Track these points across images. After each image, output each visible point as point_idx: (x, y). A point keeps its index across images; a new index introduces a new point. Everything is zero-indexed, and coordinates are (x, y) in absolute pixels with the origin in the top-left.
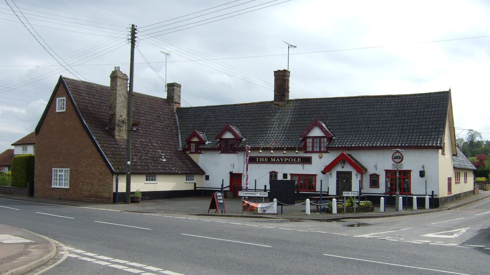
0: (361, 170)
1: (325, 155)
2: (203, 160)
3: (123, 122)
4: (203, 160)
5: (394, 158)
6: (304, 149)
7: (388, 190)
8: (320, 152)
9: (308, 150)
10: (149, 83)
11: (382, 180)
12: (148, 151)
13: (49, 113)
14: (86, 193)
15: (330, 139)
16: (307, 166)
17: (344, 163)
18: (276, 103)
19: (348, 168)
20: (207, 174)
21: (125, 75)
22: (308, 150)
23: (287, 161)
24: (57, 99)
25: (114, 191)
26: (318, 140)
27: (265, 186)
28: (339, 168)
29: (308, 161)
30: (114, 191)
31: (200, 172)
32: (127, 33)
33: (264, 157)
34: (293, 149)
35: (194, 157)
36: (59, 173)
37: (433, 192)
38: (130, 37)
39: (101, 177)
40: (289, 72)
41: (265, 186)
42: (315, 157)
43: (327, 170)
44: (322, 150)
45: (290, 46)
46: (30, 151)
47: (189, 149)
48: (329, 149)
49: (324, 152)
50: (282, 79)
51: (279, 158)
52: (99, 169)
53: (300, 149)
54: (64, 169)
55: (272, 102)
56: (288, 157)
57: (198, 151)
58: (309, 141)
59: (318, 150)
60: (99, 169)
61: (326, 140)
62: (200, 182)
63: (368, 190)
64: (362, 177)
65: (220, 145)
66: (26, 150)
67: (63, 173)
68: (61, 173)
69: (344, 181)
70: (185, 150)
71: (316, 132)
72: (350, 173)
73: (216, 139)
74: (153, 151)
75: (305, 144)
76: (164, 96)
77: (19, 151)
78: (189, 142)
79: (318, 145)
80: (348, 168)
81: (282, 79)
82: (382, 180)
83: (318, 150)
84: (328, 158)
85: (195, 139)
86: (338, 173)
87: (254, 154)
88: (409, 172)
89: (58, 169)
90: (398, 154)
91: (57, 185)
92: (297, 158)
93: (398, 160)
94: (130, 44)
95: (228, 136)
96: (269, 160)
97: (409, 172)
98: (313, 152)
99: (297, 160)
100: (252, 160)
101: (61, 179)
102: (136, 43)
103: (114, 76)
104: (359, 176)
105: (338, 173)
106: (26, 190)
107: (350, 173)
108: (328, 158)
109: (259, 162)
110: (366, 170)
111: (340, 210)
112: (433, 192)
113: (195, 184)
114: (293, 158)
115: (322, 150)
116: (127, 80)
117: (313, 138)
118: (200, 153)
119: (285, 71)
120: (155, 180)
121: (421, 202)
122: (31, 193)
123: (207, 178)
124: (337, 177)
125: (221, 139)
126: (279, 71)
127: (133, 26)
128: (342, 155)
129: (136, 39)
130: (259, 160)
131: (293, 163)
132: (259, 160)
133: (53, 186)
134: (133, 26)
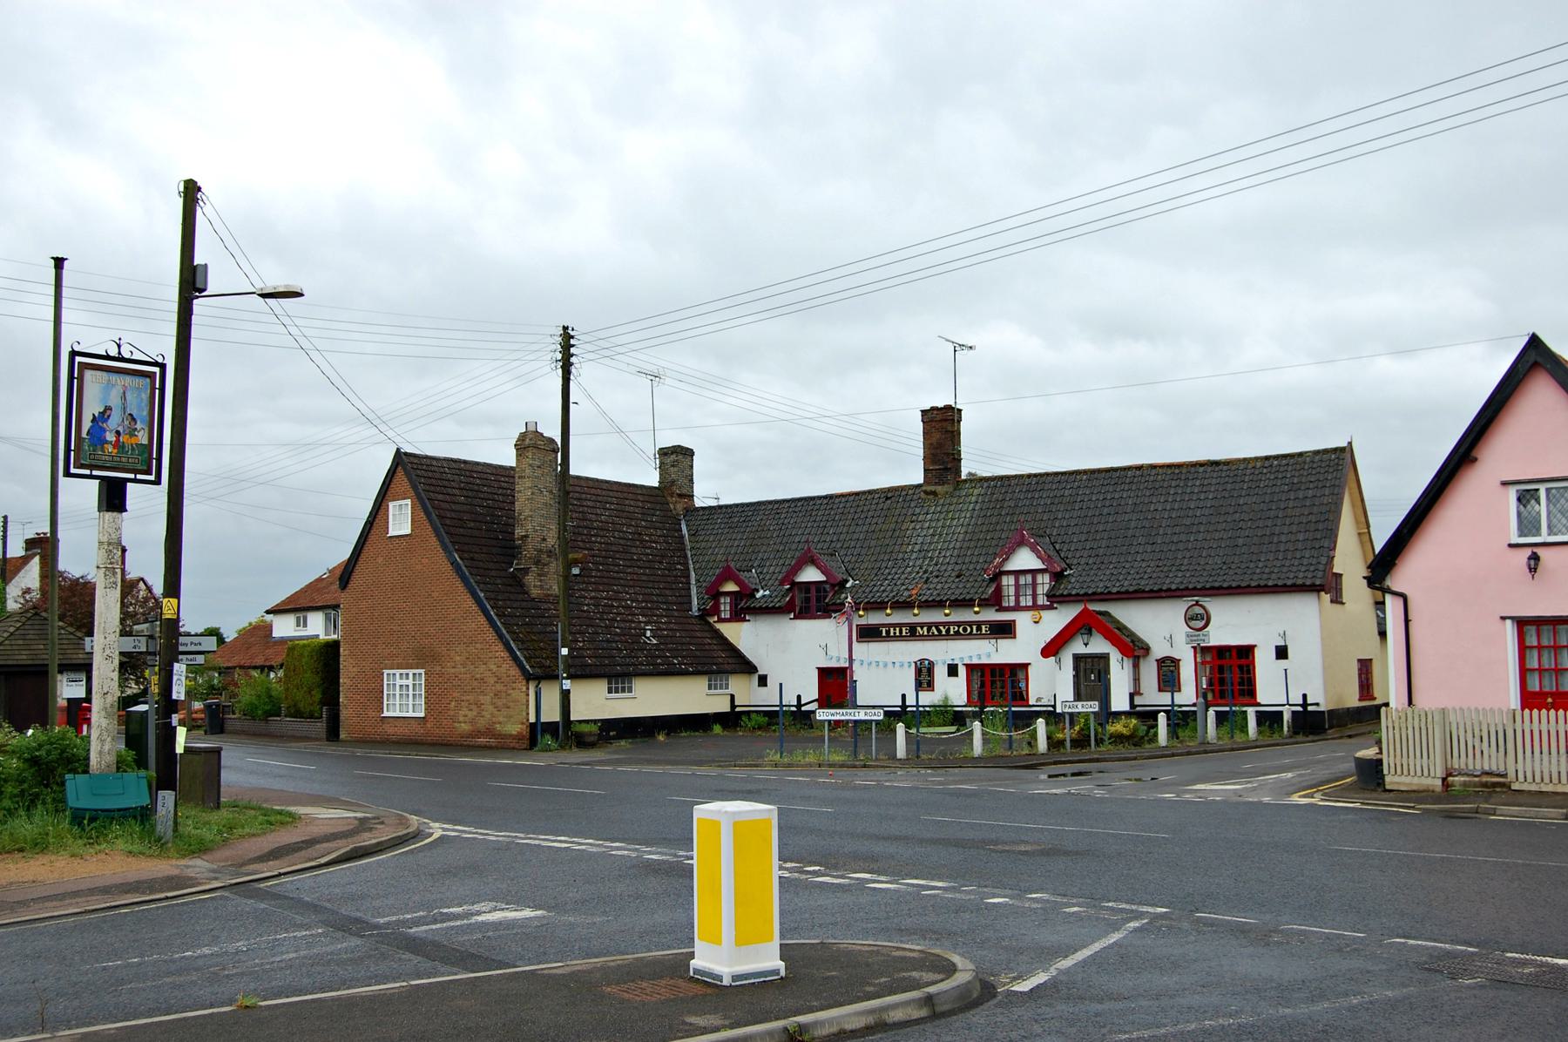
0: (1134, 649)
1: (1046, 614)
2: (746, 636)
3: (550, 553)
4: (746, 636)
5: (1189, 619)
6: (996, 601)
7: (975, 697)
8: (1035, 607)
9: (1005, 604)
10: (612, 456)
11: (1187, 672)
12: (614, 620)
13: (372, 537)
14: (465, 727)
15: (1058, 577)
16: (1004, 644)
17: (1090, 633)
18: (929, 488)
19: (1099, 645)
20: (761, 672)
21: (552, 441)
22: (1005, 604)
23: (957, 633)
24: (391, 505)
25: (532, 719)
26: (1029, 578)
27: (904, 696)
28: (1078, 647)
29: (1004, 630)
30: (532, 719)
31: (746, 667)
32: (555, 343)
33: (901, 625)
34: (966, 603)
35: (730, 630)
36: (399, 682)
37: (1305, 696)
38: (559, 356)
39: (499, 687)
40: (960, 411)
41: (904, 696)
42: (1023, 620)
43: (1052, 649)
44: (1040, 602)
45: (958, 347)
46: (316, 626)
47: (716, 610)
48: (1056, 599)
49: (1044, 608)
50: (942, 427)
51: (937, 625)
52: (493, 667)
53: (985, 603)
54: (411, 672)
55: (919, 486)
56: (959, 624)
57: (738, 616)
58: (1008, 581)
59: (1030, 603)
60: (493, 667)
61: (1047, 578)
62: (746, 693)
63: (1152, 696)
64: (1136, 666)
65: (792, 599)
66: (305, 625)
67: (410, 682)
68: (404, 682)
69: (1091, 676)
70: (704, 614)
71: (1025, 559)
72: (1105, 658)
73: (782, 583)
74: (623, 621)
75: (999, 590)
76: (652, 479)
77: (284, 627)
78: (716, 595)
79: (1029, 592)
80: (1099, 645)
81: (942, 427)
82: (1187, 672)
83: (1030, 603)
84: (1056, 621)
85: (731, 587)
86: (1078, 658)
87: (874, 619)
88: (1246, 652)
89: (398, 672)
90: (1198, 610)
91: (1538, 533)
92: (979, 624)
93: (1200, 624)
94: (560, 371)
95: (811, 575)
96: (913, 633)
97: (1246, 652)
98: (1017, 608)
99: (979, 629)
100: (869, 634)
101: (404, 696)
102: (573, 369)
103: (530, 443)
104: (1128, 663)
105: (1078, 658)
106: (320, 727)
107: (1105, 658)
108: (1056, 621)
109: (889, 638)
110: (1147, 650)
111: (1054, 744)
112: (1305, 696)
113: (732, 697)
114: (970, 624)
115: (1040, 602)
116: (555, 451)
117: (1018, 573)
118: (744, 620)
119: (948, 408)
120: (630, 690)
121: (1270, 719)
122: (333, 733)
123: (763, 681)
124: (1076, 668)
125: (794, 584)
126: (933, 409)
127: (565, 328)
128: (1085, 612)
129: (573, 360)
130: (888, 632)
131: (970, 636)
132: (888, 632)
133: (386, 714)
134: (565, 328)
